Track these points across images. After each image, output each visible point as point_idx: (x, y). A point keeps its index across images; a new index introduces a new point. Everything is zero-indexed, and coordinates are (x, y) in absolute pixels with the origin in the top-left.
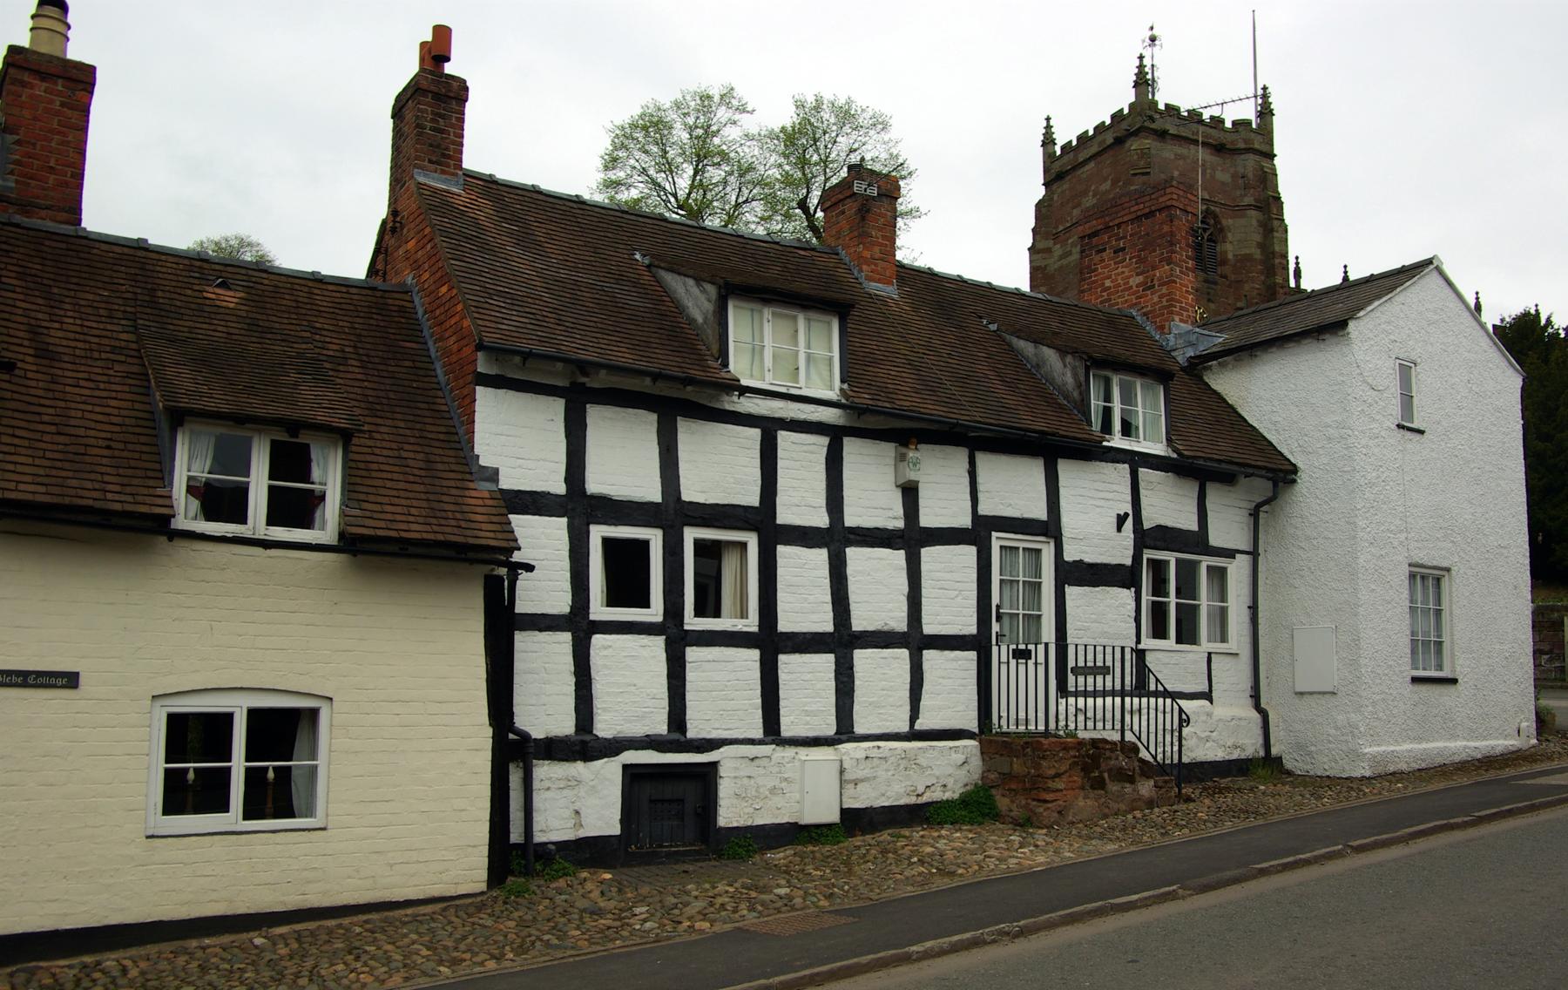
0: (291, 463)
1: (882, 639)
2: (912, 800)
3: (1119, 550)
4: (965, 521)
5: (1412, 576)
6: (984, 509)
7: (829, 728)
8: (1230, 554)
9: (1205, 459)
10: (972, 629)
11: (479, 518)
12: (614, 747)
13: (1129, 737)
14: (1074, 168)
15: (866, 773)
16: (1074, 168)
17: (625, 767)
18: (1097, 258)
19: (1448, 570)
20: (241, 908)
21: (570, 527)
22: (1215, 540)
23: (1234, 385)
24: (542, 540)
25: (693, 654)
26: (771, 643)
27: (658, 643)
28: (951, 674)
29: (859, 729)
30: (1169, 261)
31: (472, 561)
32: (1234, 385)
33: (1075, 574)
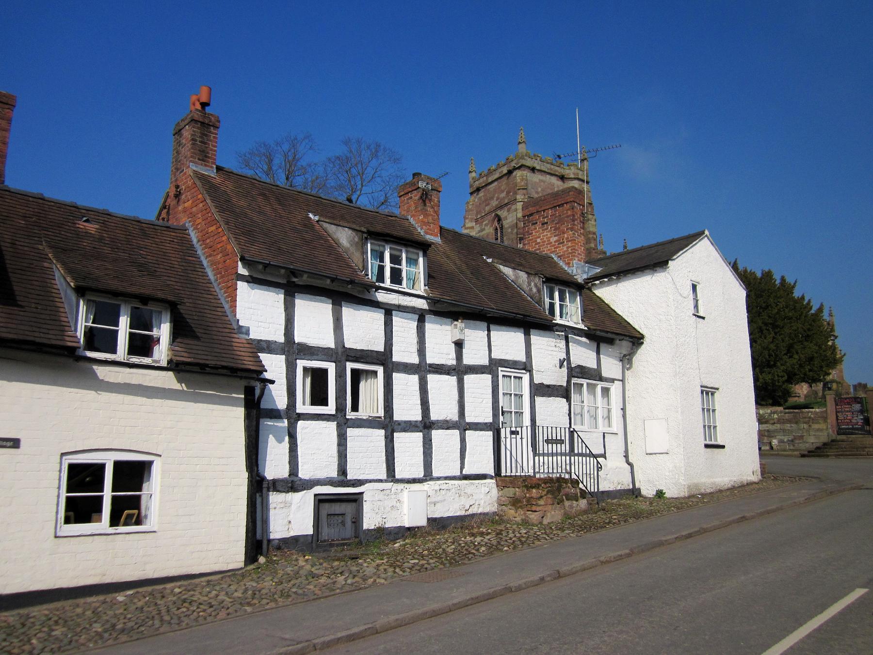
0: (140, 321)
1: (446, 425)
2: (463, 513)
3: (559, 378)
4: (486, 362)
5: (702, 392)
6: (494, 355)
7: (421, 475)
8: (612, 380)
9: (600, 331)
10: (490, 420)
11: (243, 354)
12: (308, 485)
13: (574, 476)
14: (486, 185)
15: (439, 498)
16: (486, 185)
17: (315, 495)
18: (533, 227)
19: (717, 389)
20: (108, 580)
21: (287, 361)
22: (605, 374)
23: (607, 293)
24: (274, 366)
25: (351, 432)
26: (389, 425)
27: (333, 425)
28: (480, 444)
29: (435, 474)
30: (572, 229)
31: (241, 378)
32: (607, 293)
33: (540, 390)
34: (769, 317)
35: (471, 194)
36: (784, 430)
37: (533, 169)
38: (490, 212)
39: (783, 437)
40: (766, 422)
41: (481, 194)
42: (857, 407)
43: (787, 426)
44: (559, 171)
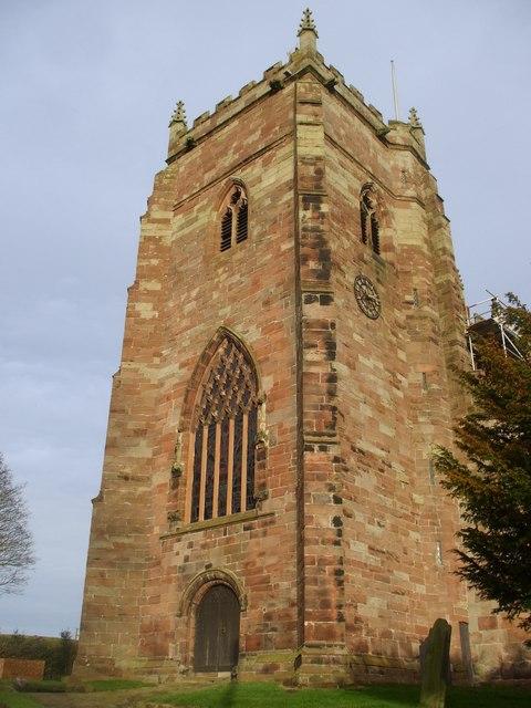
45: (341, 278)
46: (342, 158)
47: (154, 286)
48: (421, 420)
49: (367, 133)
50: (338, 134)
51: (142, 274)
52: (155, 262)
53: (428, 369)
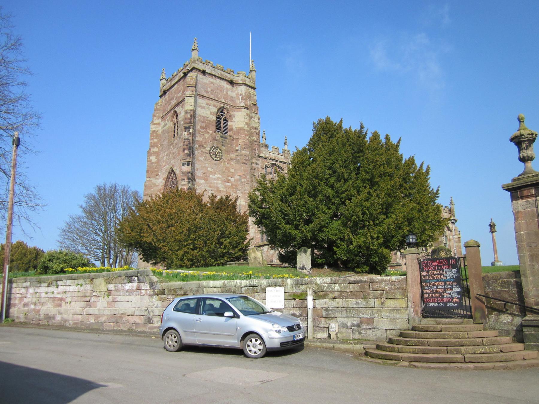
34: (367, 173)
35: (161, 97)
36: (347, 309)
37: (204, 72)
38: (171, 110)
39: (345, 320)
40: (325, 297)
41: (167, 95)
42: (451, 273)
43: (352, 303)
44: (229, 77)
45: (204, 150)
46: (208, 102)
47: (156, 150)
48: (238, 192)
49: (224, 84)
50: (207, 92)
51: (152, 145)
52: (156, 140)
53: (241, 174)
